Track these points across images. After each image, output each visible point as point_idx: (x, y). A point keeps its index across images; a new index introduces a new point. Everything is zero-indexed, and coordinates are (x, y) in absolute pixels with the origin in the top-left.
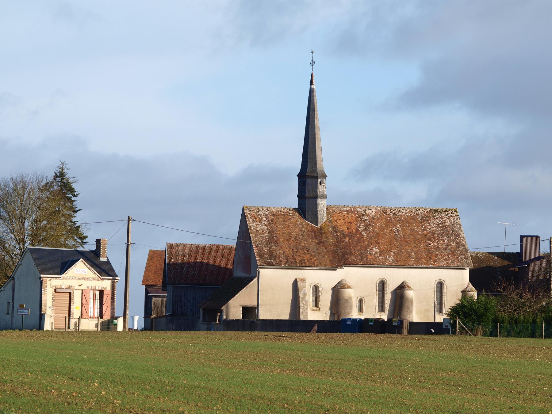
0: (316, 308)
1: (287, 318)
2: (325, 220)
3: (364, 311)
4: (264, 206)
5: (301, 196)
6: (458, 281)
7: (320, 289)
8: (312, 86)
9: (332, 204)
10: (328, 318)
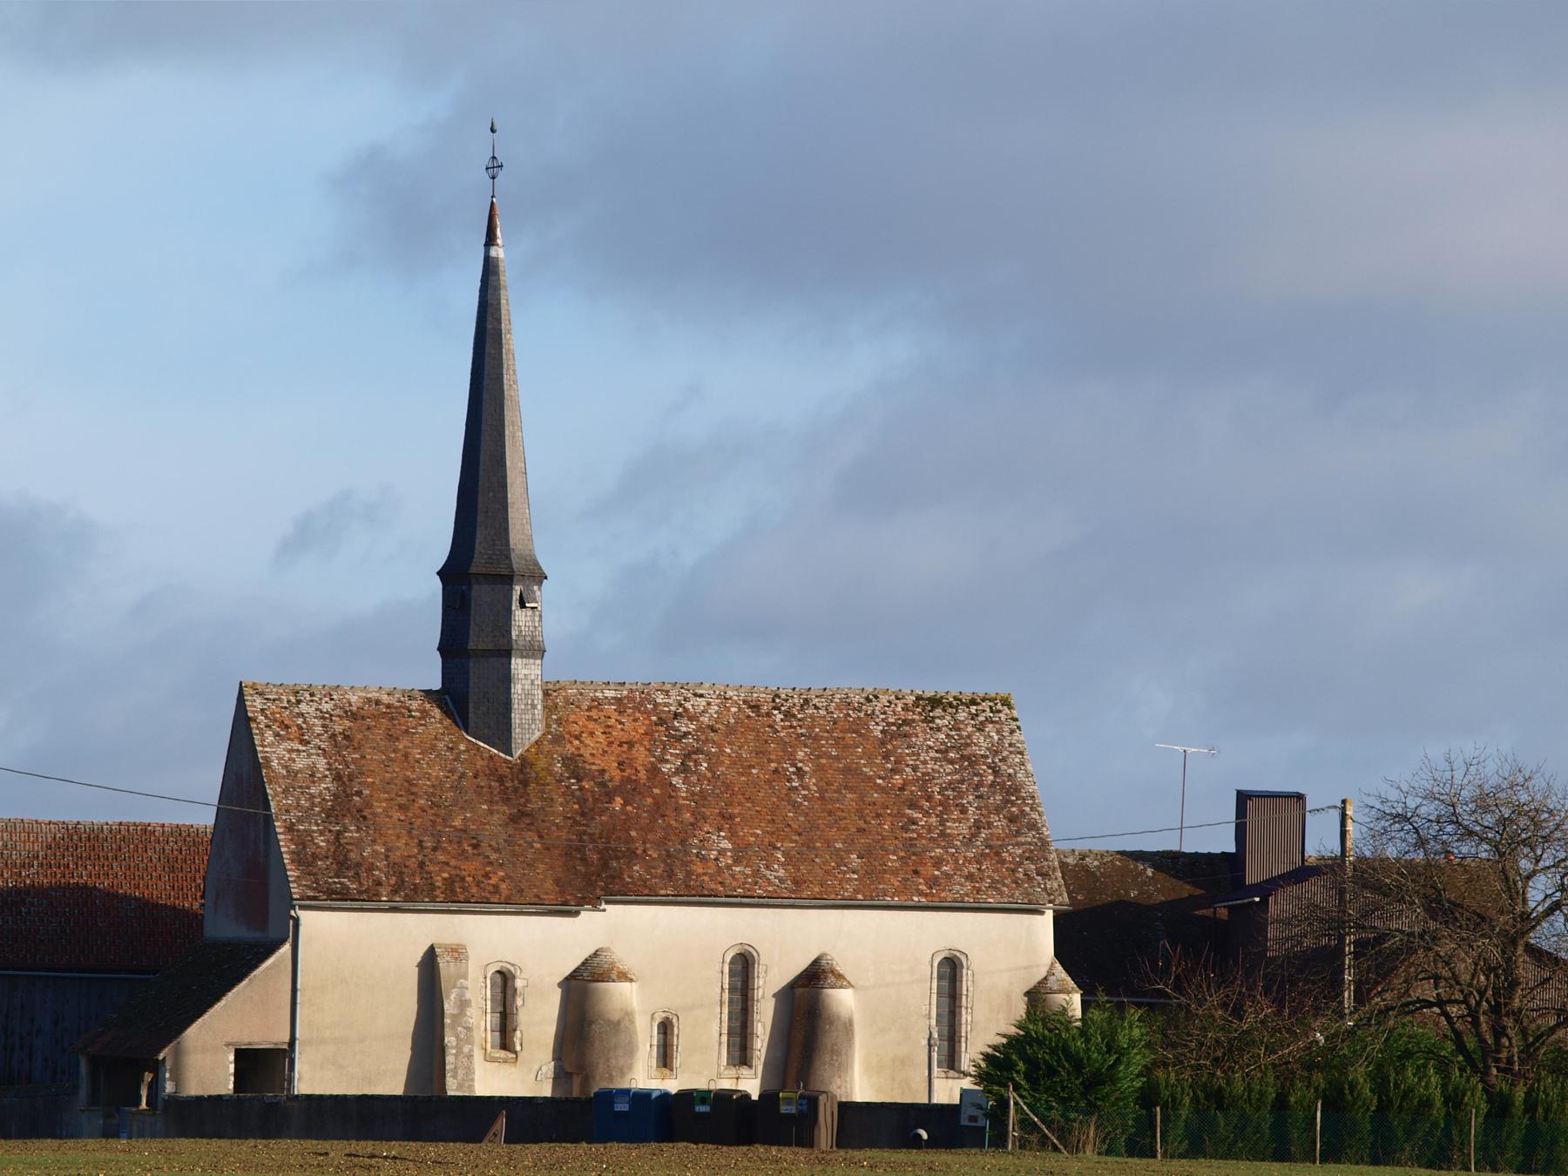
0: (503, 1054)
2: (537, 735)
4: (317, 682)
5: (453, 646)
6: (1013, 953)
7: (519, 983)
10: (546, 1091)
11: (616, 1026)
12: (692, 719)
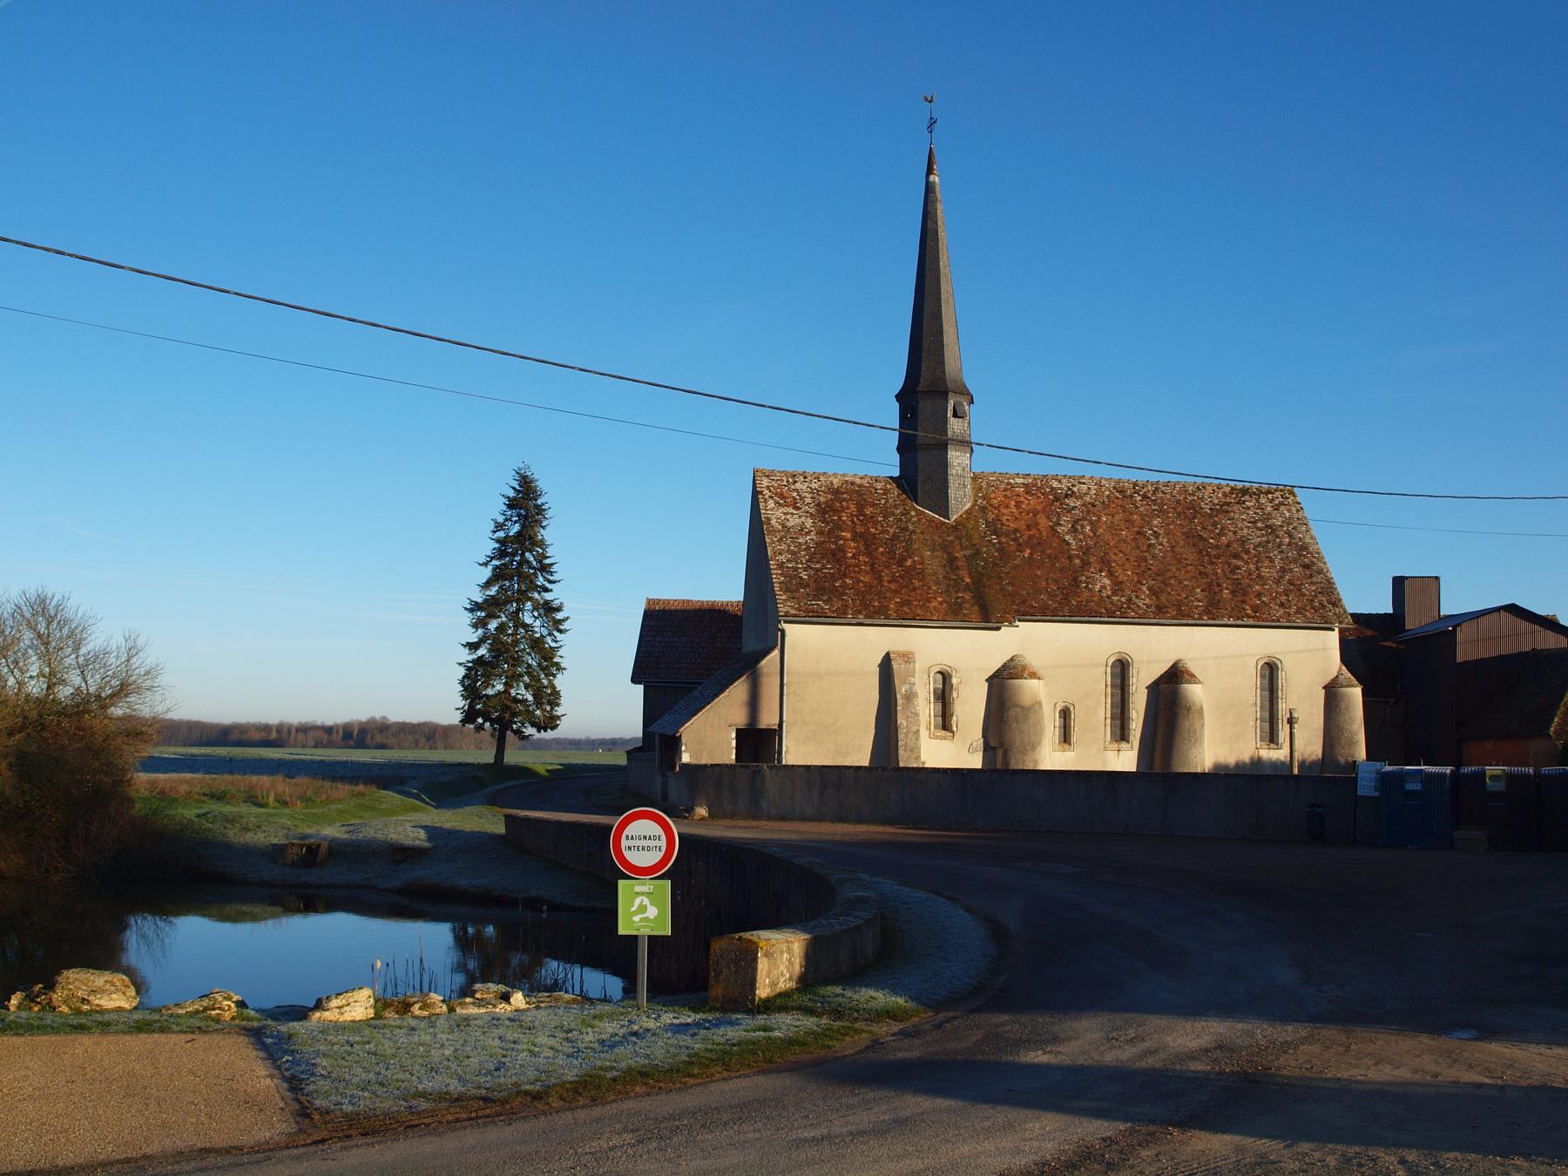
0: (943, 733)
1: (865, 761)
2: (968, 505)
3: (1074, 739)
4: (810, 470)
5: (906, 447)
6: (1311, 657)
7: (954, 681)
8: (934, 178)
10: (976, 762)
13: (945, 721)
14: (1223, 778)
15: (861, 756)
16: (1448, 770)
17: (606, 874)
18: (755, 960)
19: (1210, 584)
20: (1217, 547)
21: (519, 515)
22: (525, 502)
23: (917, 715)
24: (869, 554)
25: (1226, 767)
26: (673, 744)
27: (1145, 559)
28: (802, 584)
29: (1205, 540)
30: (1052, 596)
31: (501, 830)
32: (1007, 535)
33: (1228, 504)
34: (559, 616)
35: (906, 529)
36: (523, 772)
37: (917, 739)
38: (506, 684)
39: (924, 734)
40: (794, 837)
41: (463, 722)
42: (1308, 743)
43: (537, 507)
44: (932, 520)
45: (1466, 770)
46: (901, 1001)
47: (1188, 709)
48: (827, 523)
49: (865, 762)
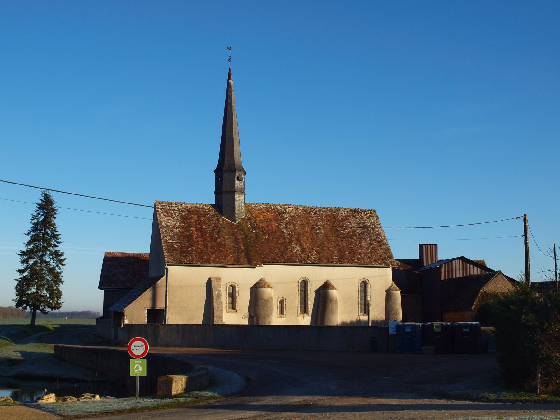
0: (232, 310)
1: (200, 322)
2: (243, 217)
3: (285, 312)
4: (178, 201)
5: (218, 192)
6: (381, 278)
7: (237, 289)
8: (231, 81)
9: (251, 202)
10: (245, 322)
11: (266, 301)
12: (289, 213)
13: (233, 306)
14: (345, 328)
15: (199, 321)
16: (420, 324)
17: (127, 357)
18: (172, 383)
19: (340, 249)
20: (344, 234)
21: (44, 212)
22: (47, 207)
23: (222, 303)
24: (202, 237)
25: (346, 323)
26: (121, 315)
27: (315, 239)
28: (175, 249)
29: (339, 231)
30: (277, 254)
31: (53, 352)
32: (259, 229)
33: (349, 216)
34: (62, 258)
35: (218, 227)
36: (43, 328)
37: (222, 313)
38: (37, 289)
39: (224, 311)
40: (173, 353)
41: (17, 306)
42: (377, 312)
43: (52, 208)
44: (228, 223)
45: (427, 324)
46: (216, 394)
47: (331, 300)
48: (185, 224)
49: (200, 322)
